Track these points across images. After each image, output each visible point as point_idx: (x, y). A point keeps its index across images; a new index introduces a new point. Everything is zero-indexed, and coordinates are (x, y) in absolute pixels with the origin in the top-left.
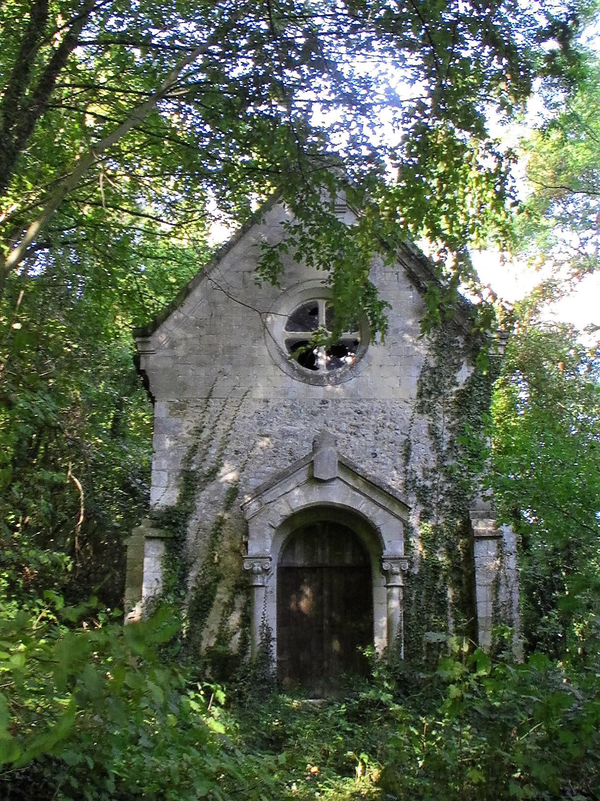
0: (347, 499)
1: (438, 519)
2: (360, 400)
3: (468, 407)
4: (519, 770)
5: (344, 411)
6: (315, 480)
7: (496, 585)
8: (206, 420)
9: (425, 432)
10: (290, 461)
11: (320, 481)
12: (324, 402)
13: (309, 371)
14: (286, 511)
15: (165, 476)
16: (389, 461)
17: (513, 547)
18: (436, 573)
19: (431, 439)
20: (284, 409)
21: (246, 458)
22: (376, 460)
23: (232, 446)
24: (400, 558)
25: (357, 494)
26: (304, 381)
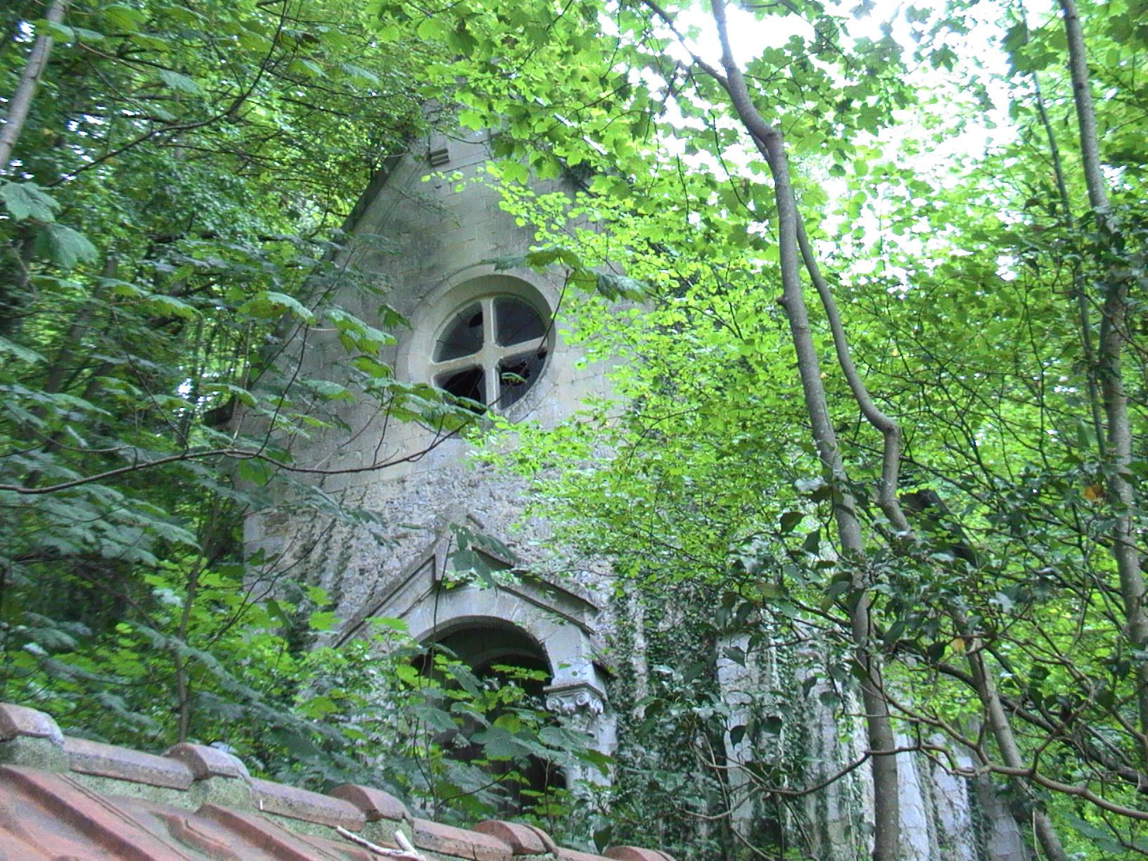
0: (492, 606)
1: (675, 616)
6: (439, 589)
8: (317, 531)
20: (428, 488)
21: (376, 576)
23: (355, 563)
25: (508, 595)
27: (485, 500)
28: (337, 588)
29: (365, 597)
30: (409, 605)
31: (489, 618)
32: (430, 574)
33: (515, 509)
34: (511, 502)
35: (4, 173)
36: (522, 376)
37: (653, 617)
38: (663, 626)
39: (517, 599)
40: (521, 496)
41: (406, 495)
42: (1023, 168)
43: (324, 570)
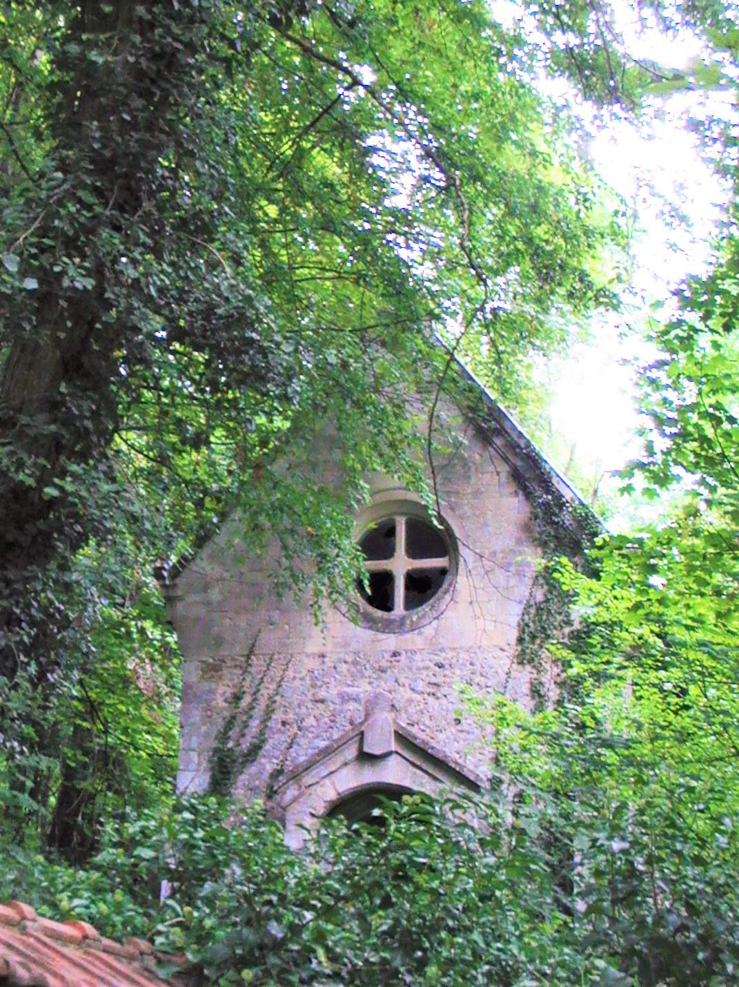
2: (442, 650)
5: (421, 665)
6: (365, 758)
8: (246, 684)
9: (526, 689)
12: (395, 654)
13: (379, 613)
19: (533, 698)
20: (344, 666)
21: (295, 730)
22: (459, 727)
23: (278, 716)
25: (418, 772)
26: (370, 628)
27: (390, 684)
28: (262, 733)
29: (286, 745)
30: (338, 765)
32: (356, 745)
33: (415, 696)
34: (412, 689)
35: (3, 19)
36: (424, 587)
40: (420, 686)
41: (325, 667)
42: (593, 546)
43: (251, 717)
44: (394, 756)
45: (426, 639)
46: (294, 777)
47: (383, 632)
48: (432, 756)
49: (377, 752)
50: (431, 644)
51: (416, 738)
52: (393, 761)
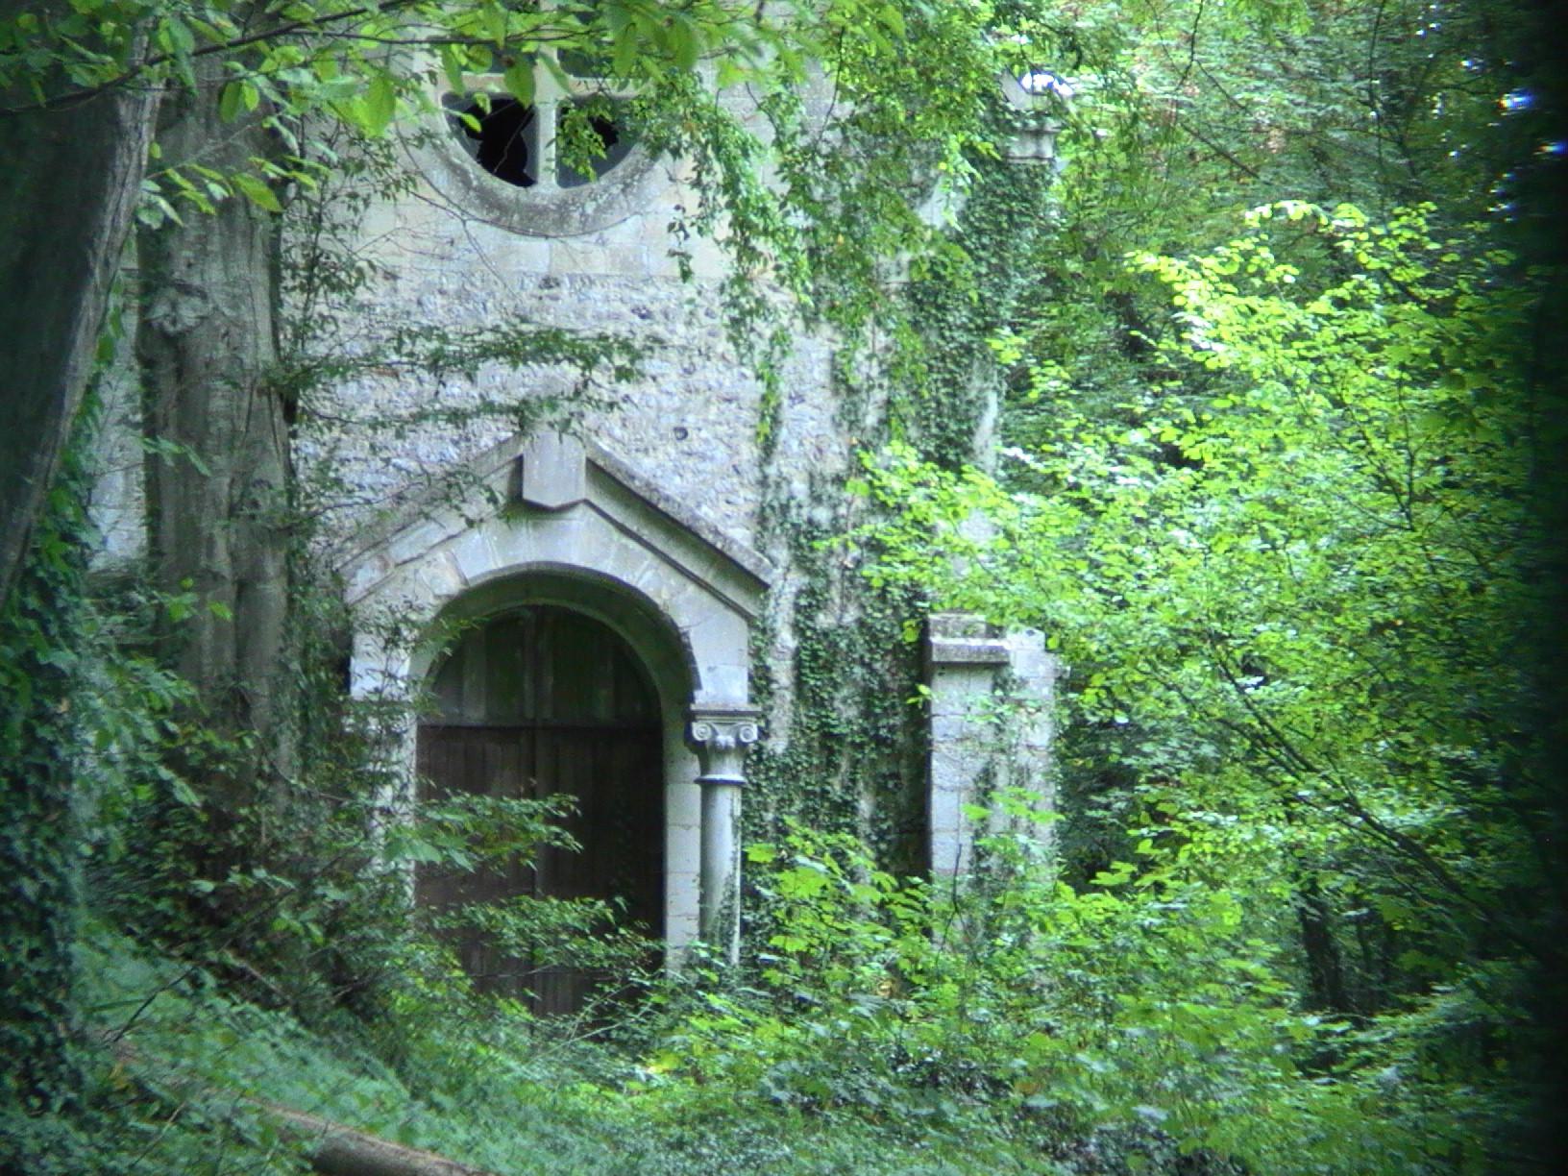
0: (606, 556)
1: (843, 609)
2: (648, 280)
3: (942, 308)
4: (267, 126)
5: (604, 309)
6: (520, 508)
7: (984, 788)
9: (820, 373)
10: (456, 443)
11: (538, 512)
12: (548, 282)
13: (508, 190)
14: (450, 584)
15: (119, 480)
16: (721, 453)
17: (1046, 691)
18: (831, 752)
19: (836, 392)
20: (439, 300)
22: (684, 445)
24: (736, 714)
25: (632, 544)
26: (495, 223)
31: (599, 574)
37: (810, 602)
38: (824, 620)
39: (649, 555)
44: (582, 509)
45: (614, 254)
46: (375, 545)
47: (524, 233)
48: (666, 515)
49: (551, 500)
50: (626, 265)
51: (633, 478)
52: (580, 520)
